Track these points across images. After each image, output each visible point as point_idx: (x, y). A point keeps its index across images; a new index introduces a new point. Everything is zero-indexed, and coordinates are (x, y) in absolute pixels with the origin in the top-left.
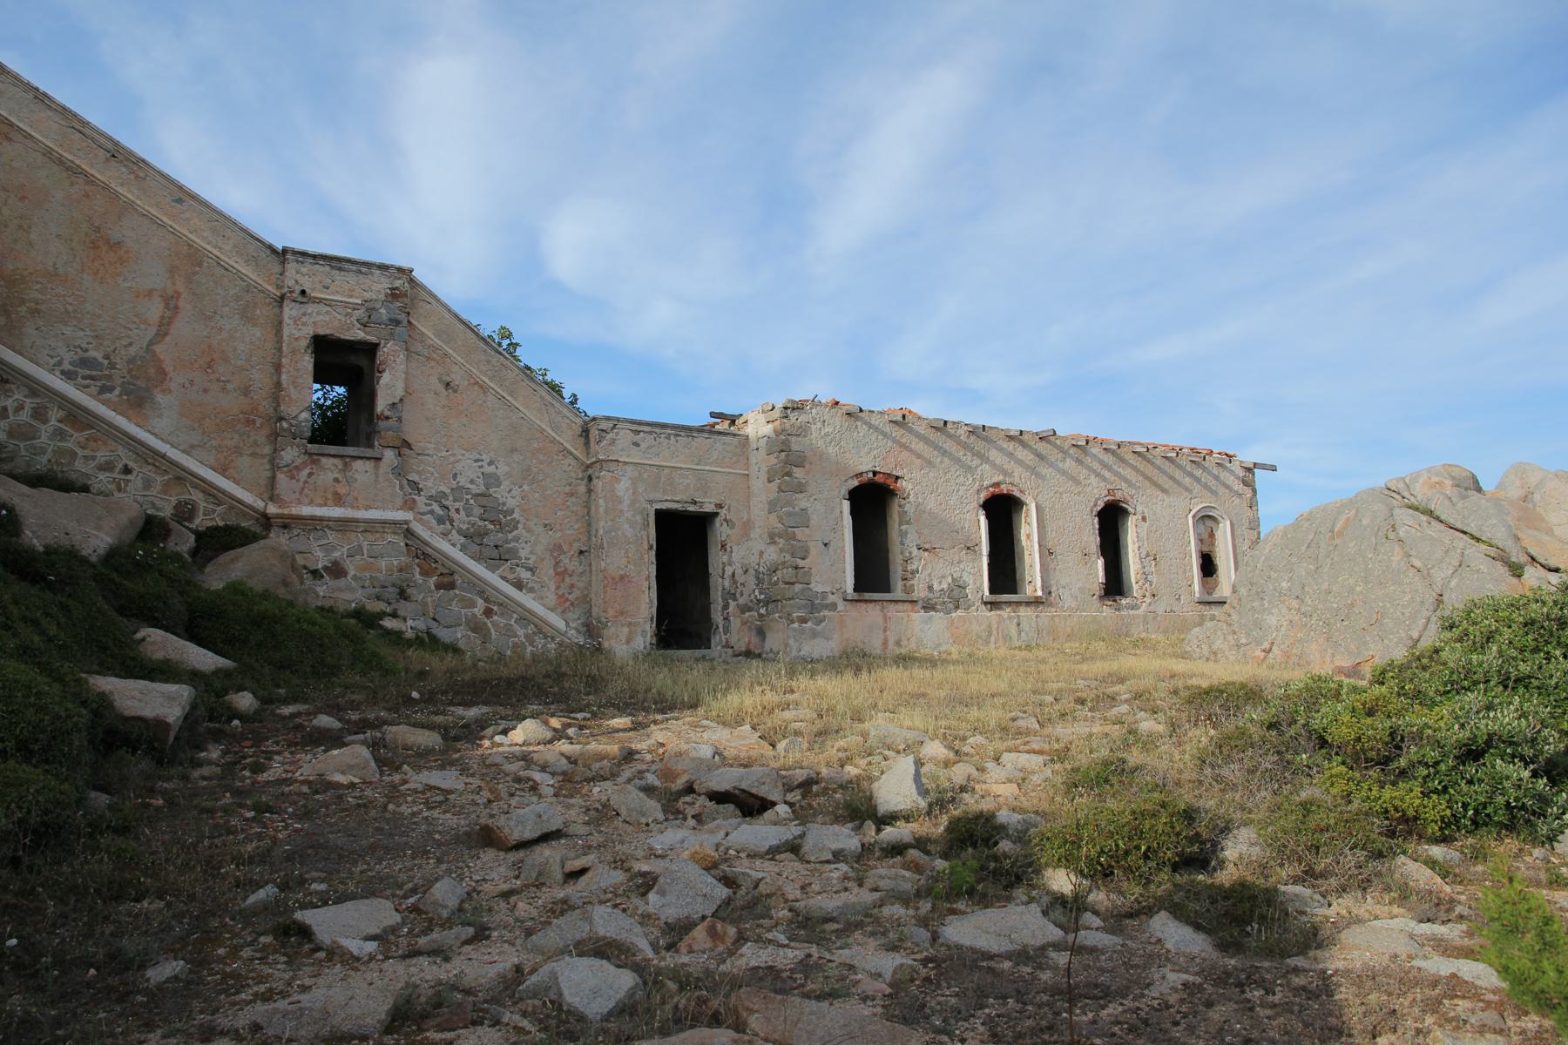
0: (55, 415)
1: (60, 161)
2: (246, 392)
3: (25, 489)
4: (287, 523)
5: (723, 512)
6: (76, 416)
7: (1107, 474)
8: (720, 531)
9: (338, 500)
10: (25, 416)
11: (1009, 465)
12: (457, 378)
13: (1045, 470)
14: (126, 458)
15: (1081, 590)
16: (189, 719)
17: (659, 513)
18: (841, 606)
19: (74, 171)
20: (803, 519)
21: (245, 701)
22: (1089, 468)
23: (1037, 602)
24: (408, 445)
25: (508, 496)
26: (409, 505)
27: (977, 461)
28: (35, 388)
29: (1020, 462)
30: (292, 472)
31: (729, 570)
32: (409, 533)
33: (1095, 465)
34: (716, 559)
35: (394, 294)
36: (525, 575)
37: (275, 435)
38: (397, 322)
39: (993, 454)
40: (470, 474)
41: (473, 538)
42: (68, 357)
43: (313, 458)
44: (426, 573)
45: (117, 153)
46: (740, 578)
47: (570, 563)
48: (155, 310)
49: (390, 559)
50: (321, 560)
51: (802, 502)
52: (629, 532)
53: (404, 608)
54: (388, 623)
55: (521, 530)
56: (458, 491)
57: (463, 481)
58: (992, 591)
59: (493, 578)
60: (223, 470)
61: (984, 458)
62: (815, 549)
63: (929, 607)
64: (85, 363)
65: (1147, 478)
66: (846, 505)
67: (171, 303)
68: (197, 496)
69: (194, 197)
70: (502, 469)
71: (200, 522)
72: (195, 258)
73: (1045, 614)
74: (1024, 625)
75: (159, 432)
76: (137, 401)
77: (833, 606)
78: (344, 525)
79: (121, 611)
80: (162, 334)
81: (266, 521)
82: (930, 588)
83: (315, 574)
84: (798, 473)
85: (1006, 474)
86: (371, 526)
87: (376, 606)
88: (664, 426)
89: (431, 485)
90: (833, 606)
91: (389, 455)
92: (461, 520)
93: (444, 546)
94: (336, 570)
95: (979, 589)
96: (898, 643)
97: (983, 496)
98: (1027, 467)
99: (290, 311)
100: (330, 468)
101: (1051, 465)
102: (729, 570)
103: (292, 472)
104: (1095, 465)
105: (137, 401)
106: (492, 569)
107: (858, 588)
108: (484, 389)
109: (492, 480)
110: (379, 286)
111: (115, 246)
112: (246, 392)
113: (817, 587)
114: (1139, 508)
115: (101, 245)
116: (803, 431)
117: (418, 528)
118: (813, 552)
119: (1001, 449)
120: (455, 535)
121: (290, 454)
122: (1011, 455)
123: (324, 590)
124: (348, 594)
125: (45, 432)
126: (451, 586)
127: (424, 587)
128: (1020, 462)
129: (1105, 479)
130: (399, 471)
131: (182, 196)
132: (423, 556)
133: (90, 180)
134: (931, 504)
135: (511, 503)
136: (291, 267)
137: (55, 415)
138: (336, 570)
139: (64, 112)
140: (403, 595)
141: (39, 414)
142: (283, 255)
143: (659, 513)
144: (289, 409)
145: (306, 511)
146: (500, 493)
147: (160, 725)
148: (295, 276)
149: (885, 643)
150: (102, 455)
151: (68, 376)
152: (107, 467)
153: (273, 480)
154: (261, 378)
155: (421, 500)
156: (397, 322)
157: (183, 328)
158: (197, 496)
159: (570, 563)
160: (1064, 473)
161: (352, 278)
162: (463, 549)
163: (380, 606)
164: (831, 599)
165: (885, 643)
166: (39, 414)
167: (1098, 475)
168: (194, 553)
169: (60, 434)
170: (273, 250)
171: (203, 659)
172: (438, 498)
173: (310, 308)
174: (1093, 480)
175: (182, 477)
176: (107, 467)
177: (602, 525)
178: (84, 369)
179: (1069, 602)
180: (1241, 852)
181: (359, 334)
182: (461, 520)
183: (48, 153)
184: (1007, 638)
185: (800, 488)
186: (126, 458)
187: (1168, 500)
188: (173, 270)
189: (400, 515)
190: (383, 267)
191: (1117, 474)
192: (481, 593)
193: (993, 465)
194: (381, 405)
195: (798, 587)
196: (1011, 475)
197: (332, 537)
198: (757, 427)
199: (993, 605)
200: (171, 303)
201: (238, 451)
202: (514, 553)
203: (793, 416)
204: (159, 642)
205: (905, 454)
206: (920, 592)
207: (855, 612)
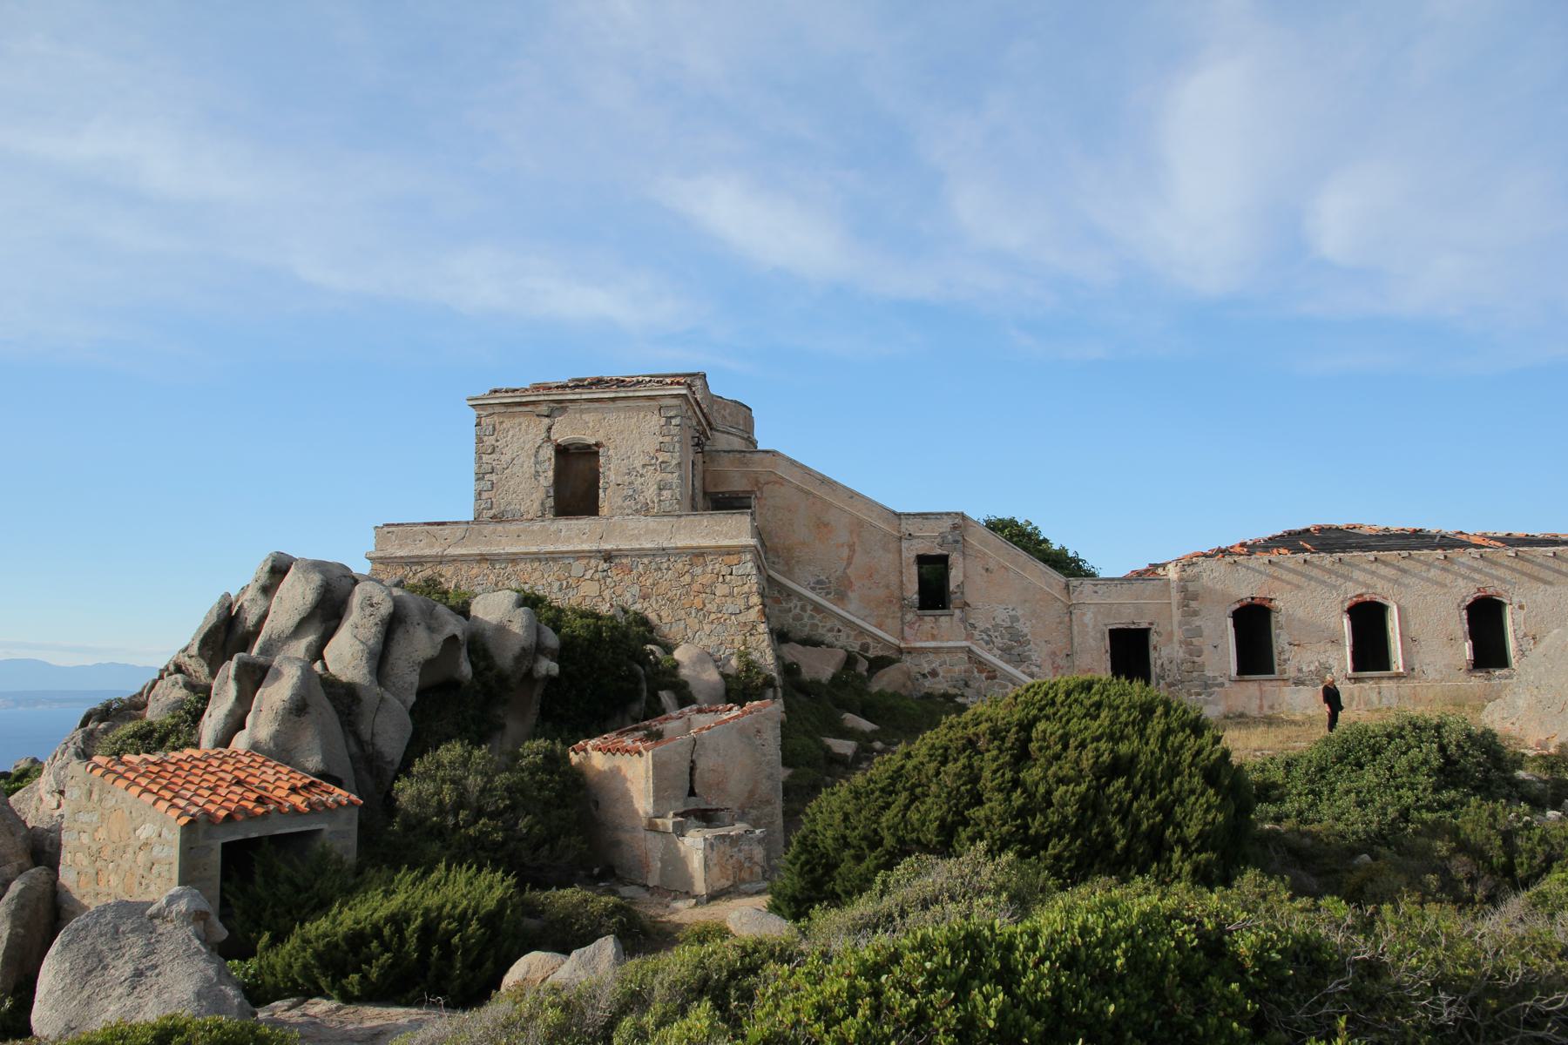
0: (809, 608)
1: (802, 490)
2: (888, 587)
3: (800, 647)
4: (910, 651)
5: (1154, 627)
6: (818, 608)
7: (1477, 576)
8: (1154, 639)
9: (934, 637)
10: (798, 610)
11: (1368, 579)
12: (991, 566)
13: (1407, 580)
14: (838, 625)
15: (1447, 666)
16: (856, 754)
17: (1111, 631)
18: (1227, 684)
19: (808, 493)
20: (1198, 632)
21: (878, 745)
22: (1456, 574)
23: (1398, 676)
24: (967, 604)
25: (1024, 627)
26: (969, 637)
27: (1341, 581)
28: (801, 597)
29: (1383, 577)
30: (911, 625)
31: (1159, 662)
32: (970, 651)
33: (1463, 571)
34: (1153, 655)
35: (955, 527)
36: (1035, 669)
37: (902, 607)
38: (957, 542)
39: (1356, 574)
40: (1002, 616)
41: (1006, 652)
42: (813, 580)
43: (920, 618)
44: (980, 672)
45: (824, 481)
46: (1167, 666)
47: (1061, 662)
48: (845, 552)
49: (960, 666)
50: (926, 669)
51: (1197, 622)
52: (1093, 643)
53: (967, 691)
54: (959, 700)
55: (1032, 645)
56: (996, 627)
57: (998, 621)
58: (1355, 669)
59: (1017, 673)
60: (879, 626)
61: (1347, 578)
62: (1207, 650)
63: (1299, 682)
64: (819, 582)
65: (1524, 574)
66: (1230, 622)
67: (852, 547)
68: (869, 640)
69: (858, 494)
70: (1020, 612)
71: (871, 654)
72: (860, 523)
73: (1406, 687)
74: (1384, 692)
75: (851, 611)
76: (841, 597)
77: (1222, 685)
78: (937, 650)
79: (838, 706)
80: (849, 564)
81: (900, 651)
82: (1300, 670)
83: (924, 676)
84: (1193, 604)
85: (1368, 586)
86: (950, 650)
87: (952, 691)
88: (1113, 579)
89: (981, 625)
90: (1222, 685)
91: (957, 612)
92: (998, 641)
93: (989, 657)
94: (934, 673)
95: (1345, 668)
96: (1272, 707)
97: (1347, 605)
98: (1389, 580)
99: (905, 544)
100: (928, 620)
101: (1415, 575)
102: (1159, 662)
103: (911, 625)
104: (1463, 571)
105: (841, 597)
106: (1016, 667)
107: (1240, 673)
108: (1006, 569)
109: (1014, 619)
110: (947, 524)
111: (826, 525)
112: (888, 587)
113: (1209, 674)
114: (1515, 600)
115: (822, 525)
116: (1197, 577)
117: (975, 648)
118: (1206, 652)
119: (1364, 570)
120: (996, 651)
121: (909, 617)
122: (1373, 573)
123: (928, 685)
124: (940, 686)
125: (805, 616)
126: (995, 677)
127: (980, 679)
128: (1383, 577)
129: (1474, 580)
130: (963, 620)
131: (853, 495)
132: (980, 664)
133: (814, 496)
134: (1300, 613)
135: (1026, 630)
136: (904, 522)
137: (809, 608)
138: (934, 673)
139: (802, 467)
140: (967, 685)
141: (803, 609)
142: (898, 515)
143: (1111, 631)
144: (907, 594)
145: (918, 645)
146: (1018, 626)
147: (845, 756)
148: (908, 526)
149: (1261, 707)
150: (829, 625)
151: (813, 589)
152: (831, 630)
153: (902, 630)
154: (894, 579)
155: (976, 633)
156: (957, 542)
157: (858, 559)
158: (869, 640)
159: (1061, 662)
160: (1428, 580)
161: (932, 522)
162: (1001, 657)
163: (955, 691)
164: (1220, 680)
165: (1261, 707)
166: (803, 609)
167: (1464, 577)
168: (868, 670)
169: (812, 617)
170: (894, 513)
171: (866, 725)
172: (986, 631)
173: (914, 542)
174: (1461, 582)
175: (862, 632)
176: (831, 630)
177: (1076, 641)
178: (819, 585)
179: (1432, 674)
180: (979, 813)
181: (938, 551)
182: (998, 641)
183: (797, 488)
184: (1368, 702)
185: (1195, 613)
186: (838, 625)
187: (1550, 589)
188: (851, 532)
189: (964, 644)
190: (948, 514)
191: (1487, 574)
192: (1011, 681)
193: (1357, 582)
194: (952, 587)
195: (1195, 674)
196: (1374, 587)
197: (931, 656)
198: (1173, 573)
199: (1357, 680)
200: (852, 547)
201: (886, 616)
202: (1029, 658)
203: (1189, 570)
204: (852, 720)
205: (1277, 583)
206: (1291, 672)
207: (1237, 687)
